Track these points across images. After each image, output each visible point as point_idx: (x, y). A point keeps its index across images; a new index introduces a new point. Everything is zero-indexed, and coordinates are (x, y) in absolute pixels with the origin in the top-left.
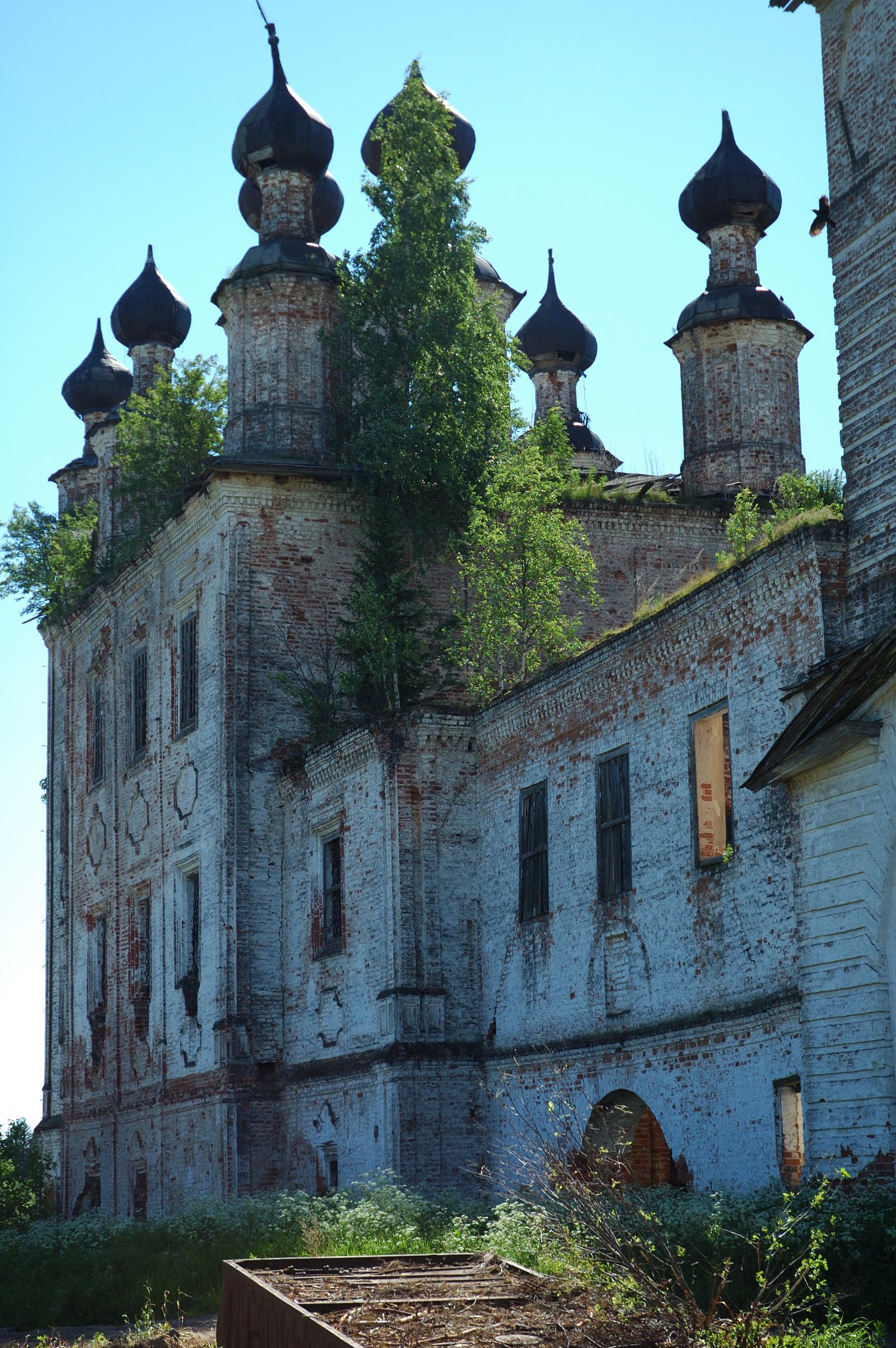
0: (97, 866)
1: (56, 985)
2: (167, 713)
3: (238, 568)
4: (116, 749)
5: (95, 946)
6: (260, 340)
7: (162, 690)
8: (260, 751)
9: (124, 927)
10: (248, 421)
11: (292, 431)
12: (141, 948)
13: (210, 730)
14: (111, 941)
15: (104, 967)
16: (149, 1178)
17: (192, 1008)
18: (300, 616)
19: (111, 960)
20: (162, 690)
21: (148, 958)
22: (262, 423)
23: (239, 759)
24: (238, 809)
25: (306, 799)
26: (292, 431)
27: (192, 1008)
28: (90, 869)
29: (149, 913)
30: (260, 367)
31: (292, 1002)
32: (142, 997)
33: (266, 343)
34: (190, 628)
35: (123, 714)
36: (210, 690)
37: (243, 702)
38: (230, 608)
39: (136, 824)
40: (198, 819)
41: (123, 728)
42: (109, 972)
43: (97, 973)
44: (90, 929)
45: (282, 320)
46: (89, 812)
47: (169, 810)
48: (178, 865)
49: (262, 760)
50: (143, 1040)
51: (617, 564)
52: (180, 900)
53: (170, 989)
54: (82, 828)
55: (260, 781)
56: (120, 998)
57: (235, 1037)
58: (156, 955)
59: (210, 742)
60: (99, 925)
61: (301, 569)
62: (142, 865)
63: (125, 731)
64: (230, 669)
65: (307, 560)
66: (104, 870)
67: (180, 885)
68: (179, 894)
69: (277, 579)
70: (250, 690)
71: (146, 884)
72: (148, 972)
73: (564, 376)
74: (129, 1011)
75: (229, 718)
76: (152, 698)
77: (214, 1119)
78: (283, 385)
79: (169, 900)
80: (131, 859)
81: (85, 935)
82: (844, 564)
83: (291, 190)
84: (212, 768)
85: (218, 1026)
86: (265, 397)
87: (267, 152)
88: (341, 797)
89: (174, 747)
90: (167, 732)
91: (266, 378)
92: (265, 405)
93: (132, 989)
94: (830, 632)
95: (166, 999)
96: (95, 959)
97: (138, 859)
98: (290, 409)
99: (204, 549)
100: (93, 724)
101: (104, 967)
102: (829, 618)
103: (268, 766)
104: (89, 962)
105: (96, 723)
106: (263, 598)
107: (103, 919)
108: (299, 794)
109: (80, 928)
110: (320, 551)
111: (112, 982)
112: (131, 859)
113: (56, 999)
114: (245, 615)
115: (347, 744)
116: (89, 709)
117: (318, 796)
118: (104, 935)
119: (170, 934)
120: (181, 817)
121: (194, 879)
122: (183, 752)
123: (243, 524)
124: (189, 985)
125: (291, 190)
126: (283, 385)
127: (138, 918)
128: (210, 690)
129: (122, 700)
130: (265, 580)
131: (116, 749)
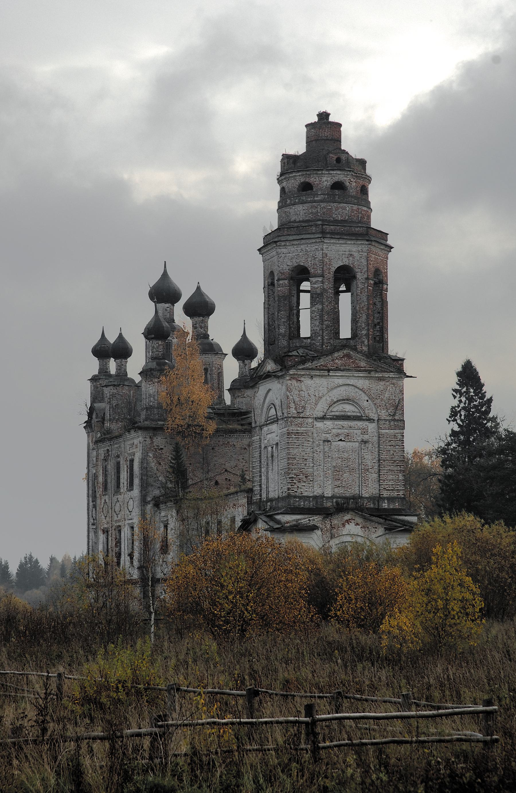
0: (106, 517)
1: (90, 543)
2: (126, 483)
3: (144, 452)
4: (111, 484)
5: (105, 539)
6: (150, 388)
7: (124, 476)
8: (149, 499)
9: (114, 536)
10: (147, 410)
11: (158, 414)
12: (118, 543)
13: (136, 492)
14: (110, 539)
15: (108, 545)
16: (121, 463)
17: (132, 563)
18: (160, 464)
19: (110, 544)
20: (124, 476)
21: (120, 545)
22: (151, 411)
23: (144, 501)
24: (143, 515)
25: (160, 513)
26: (158, 414)
27: (132, 563)
28: (103, 517)
29: (120, 533)
30: (150, 395)
31: (156, 562)
32: (119, 555)
33: (152, 389)
34: (132, 461)
35: (113, 477)
36: (137, 481)
37: (145, 487)
38: (142, 462)
39: (117, 509)
40: (133, 514)
41: (113, 481)
42: (109, 547)
43: (106, 546)
44: (103, 534)
45: (156, 384)
46: (103, 501)
47: (126, 509)
48: (129, 524)
49: (150, 501)
50: (119, 567)
51: (245, 446)
52: (129, 533)
53: (126, 556)
54: (101, 504)
55: (149, 507)
56: (112, 555)
57: (143, 571)
58: (122, 546)
59: (136, 495)
60: (106, 533)
61: (160, 451)
62: (119, 521)
63: (114, 482)
64: (142, 478)
65: (162, 449)
66: (107, 518)
67: (129, 529)
68: (129, 531)
69: (154, 455)
70: (146, 484)
71: (120, 526)
72: (120, 549)
73: (246, 362)
74: (115, 560)
75: (141, 491)
76: (122, 476)
77: (137, 591)
78: (156, 401)
79: (126, 532)
80: (115, 518)
81: (102, 535)
82: (251, 498)
83: (159, 345)
84: (137, 502)
85: (138, 568)
86: (151, 404)
87: (153, 336)
88: (167, 516)
89: (127, 492)
90: (126, 488)
91: (152, 399)
92: (151, 406)
93: (116, 553)
94: (248, 510)
95: (125, 559)
96: (105, 542)
97: (117, 519)
98: (158, 408)
99: (135, 443)
100: (104, 475)
101: (108, 545)
102: (248, 507)
103: (151, 503)
104: (103, 543)
105: (105, 475)
106: (150, 459)
107: (107, 532)
108: (159, 511)
109: (100, 533)
110: (165, 447)
111: (110, 550)
112: (115, 518)
113: (91, 547)
114: (145, 464)
115: (169, 504)
116: (103, 470)
117: (163, 514)
118: (108, 536)
119: (126, 541)
120: (129, 512)
121: (132, 528)
122: (130, 495)
123: (145, 440)
124: (131, 555)
125: (159, 345)
126: (156, 401)
127: (118, 534)
128: (137, 481)
129: (113, 473)
130: (151, 455)
131: (111, 484)
